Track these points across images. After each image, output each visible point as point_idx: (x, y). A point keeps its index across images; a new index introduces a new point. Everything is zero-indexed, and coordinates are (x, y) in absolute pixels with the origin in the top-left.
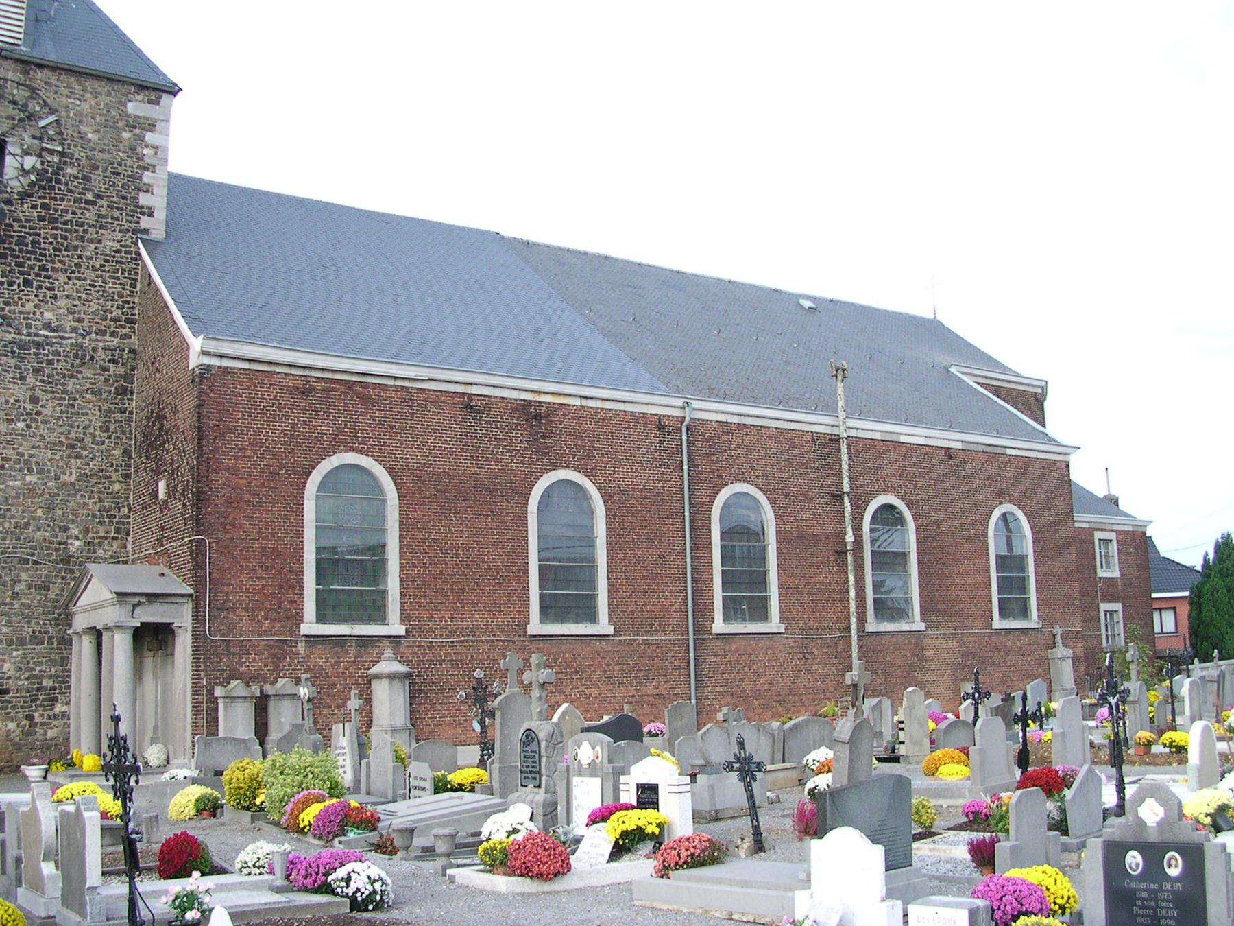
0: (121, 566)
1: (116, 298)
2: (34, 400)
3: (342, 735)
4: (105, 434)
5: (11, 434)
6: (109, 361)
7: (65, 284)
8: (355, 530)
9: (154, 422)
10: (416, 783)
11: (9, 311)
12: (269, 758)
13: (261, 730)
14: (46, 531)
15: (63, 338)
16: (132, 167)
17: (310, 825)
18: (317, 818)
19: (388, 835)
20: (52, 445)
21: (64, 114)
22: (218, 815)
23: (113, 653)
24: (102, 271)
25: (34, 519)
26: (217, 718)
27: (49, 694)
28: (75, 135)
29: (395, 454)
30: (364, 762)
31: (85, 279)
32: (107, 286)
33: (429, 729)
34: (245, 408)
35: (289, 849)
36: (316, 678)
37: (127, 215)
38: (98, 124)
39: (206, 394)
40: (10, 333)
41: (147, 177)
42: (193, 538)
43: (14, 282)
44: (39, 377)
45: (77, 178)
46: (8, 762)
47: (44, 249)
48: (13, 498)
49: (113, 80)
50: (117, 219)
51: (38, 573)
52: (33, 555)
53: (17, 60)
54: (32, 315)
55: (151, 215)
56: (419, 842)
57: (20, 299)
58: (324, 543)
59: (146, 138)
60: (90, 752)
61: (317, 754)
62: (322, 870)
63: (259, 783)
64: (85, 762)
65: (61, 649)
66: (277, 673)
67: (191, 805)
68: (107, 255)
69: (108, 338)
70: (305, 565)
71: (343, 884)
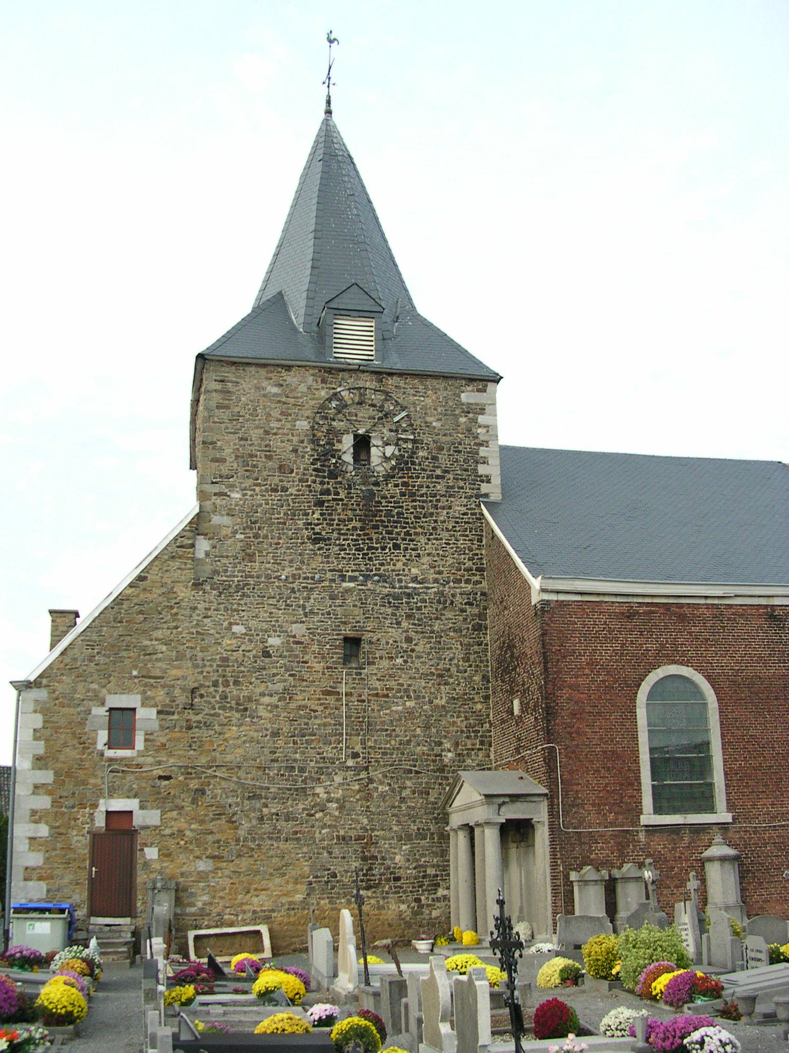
0: (487, 772)
1: (467, 552)
2: (409, 640)
3: (683, 913)
4: (467, 664)
5: (392, 669)
6: (466, 604)
7: (426, 544)
8: (681, 731)
9: (506, 651)
10: (753, 955)
11: (384, 570)
12: (622, 935)
13: (611, 908)
14: (424, 746)
15: (428, 588)
16: (470, 445)
17: (662, 993)
18: (668, 986)
19: (732, 1001)
20: (424, 676)
21: (412, 409)
22: (580, 983)
23: (484, 845)
24: (454, 531)
25: (415, 736)
26: (573, 899)
27: (432, 881)
28: (423, 424)
29: (711, 663)
30: (705, 936)
31: (441, 539)
32: (459, 543)
33: (758, 905)
34: (580, 634)
35: (647, 1014)
36: (658, 862)
37: (470, 483)
38: (440, 414)
39: (548, 624)
40: (386, 587)
41: (483, 451)
42: (545, 746)
43: (386, 547)
44: (411, 621)
45: (427, 458)
46: (401, 937)
47: (408, 518)
48: (397, 720)
49: (447, 377)
50: (462, 488)
51: (420, 780)
52: (415, 766)
53: (372, 372)
54: (402, 572)
55: (489, 481)
56: (760, 1008)
57: (391, 560)
58: (656, 744)
59: (479, 420)
60: (468, 929)
61: (664, 930)
62: (678, 1034)
63: (614, 956)
64: (464, 937)
65: (441, 843)
66: (623, 858)
67: (557, 975)
68: (457, 518)
69: (463, 585)
70: (641, 764)
71: (697, 1046)
